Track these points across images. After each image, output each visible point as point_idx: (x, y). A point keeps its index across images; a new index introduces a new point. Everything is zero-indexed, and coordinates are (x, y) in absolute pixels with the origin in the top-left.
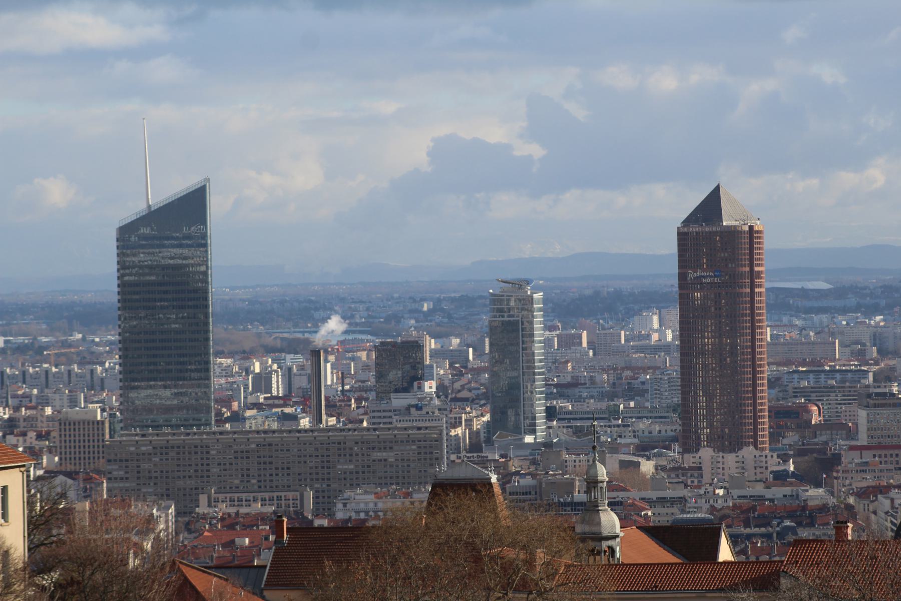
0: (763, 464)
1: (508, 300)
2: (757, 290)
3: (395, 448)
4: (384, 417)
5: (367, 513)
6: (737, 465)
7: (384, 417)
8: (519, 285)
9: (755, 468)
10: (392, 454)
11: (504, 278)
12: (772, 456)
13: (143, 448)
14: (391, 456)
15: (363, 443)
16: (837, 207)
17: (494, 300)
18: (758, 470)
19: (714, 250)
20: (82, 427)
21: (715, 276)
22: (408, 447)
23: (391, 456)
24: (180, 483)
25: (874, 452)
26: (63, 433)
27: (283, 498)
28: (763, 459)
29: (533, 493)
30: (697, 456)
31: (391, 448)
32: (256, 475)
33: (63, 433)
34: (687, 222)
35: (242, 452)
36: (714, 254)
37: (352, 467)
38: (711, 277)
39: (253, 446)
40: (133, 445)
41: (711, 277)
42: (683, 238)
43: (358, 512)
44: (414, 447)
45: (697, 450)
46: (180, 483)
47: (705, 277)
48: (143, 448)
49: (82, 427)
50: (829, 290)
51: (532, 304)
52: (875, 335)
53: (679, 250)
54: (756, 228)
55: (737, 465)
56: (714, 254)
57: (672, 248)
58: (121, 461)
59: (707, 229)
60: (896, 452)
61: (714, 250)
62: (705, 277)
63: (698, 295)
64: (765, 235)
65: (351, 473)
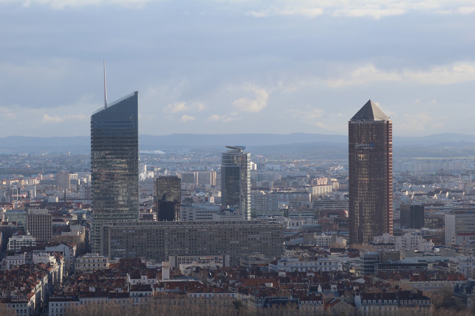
0: (416, 242)
1: (233, 157)
2: (390, 153)
3: (260, 233)
4: (203, 215)
5: (306, 268)
6: (402, 242)
7: (203, 215)
8: (237, 149)
9: (411, 244)
10: (258, 236)
11: (231, 146)
12: (420, 238)
13: (130, 231)
14: (258, 237)
15: (243, 230)
16: (433, 114)
17: (224, 157)
18: (413, 245)
19: (369, 133)
20: (40, 218)
21: (370, 146)
22: (267, 233)
23: (258, 237)
24: (149, 250)
25: (471, 236)
26: (30, 224)
27: (186, 259)
28: (415, 239)
29: (377, 258)
30: (382, 238)
31: (258, 233)
32: (188, 246)
33: (30, 224)
34: (354, 118)
35: (181, 234)
36: (369, 134)
37: (238, 242)
38: (368, 146)
39: (187, 231)
40: (124, 230)
41: (368, 146)
42: (352, 127)
43: (292, 268)
44: (270, 232)
45: (382, 235)
46: (149, 250)
47: (365, 146)
48: (130, 231)
49: (40, 218)
50: (163, 155)
51: (247, 159)
52: (259, 176)
53: (349, 133)
54: (390, 123)
55: (402, 242)
56: (369, 134)
57: (345, 131)
58: (118, 238)
59: (366, 122)
60: (474, 236)
61: (369, 133)
62: (365, 146)
63: (362, 156)
64: (393, 126)
65: (237, 245)
